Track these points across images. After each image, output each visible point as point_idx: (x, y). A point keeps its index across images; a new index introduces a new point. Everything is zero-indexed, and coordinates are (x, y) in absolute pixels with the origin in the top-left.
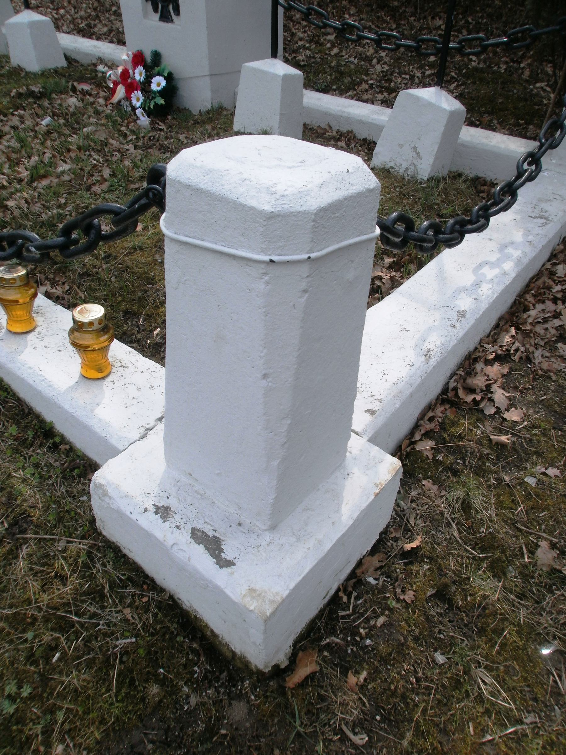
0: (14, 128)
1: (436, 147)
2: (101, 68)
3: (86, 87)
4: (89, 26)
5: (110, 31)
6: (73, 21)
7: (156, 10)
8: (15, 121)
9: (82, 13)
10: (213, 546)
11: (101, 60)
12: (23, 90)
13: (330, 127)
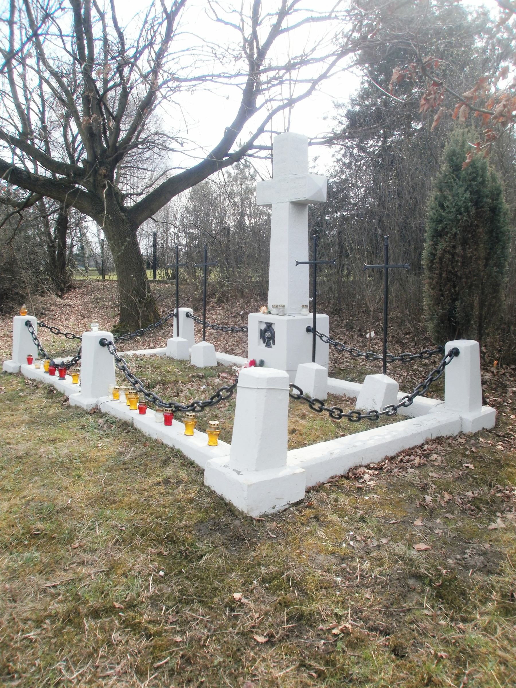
0: (189, 389)
1: (382, 399)
2: (234, 368)
3: (225, 375)
4: (232, 349)
5: (243, 352)
6: (224, 347)
7: (264, 342)
8: (189, 386)
9: (230, 343)
10: (239, 473)
11: (235, 364)
12: (195, 374)
13: (345, 396)
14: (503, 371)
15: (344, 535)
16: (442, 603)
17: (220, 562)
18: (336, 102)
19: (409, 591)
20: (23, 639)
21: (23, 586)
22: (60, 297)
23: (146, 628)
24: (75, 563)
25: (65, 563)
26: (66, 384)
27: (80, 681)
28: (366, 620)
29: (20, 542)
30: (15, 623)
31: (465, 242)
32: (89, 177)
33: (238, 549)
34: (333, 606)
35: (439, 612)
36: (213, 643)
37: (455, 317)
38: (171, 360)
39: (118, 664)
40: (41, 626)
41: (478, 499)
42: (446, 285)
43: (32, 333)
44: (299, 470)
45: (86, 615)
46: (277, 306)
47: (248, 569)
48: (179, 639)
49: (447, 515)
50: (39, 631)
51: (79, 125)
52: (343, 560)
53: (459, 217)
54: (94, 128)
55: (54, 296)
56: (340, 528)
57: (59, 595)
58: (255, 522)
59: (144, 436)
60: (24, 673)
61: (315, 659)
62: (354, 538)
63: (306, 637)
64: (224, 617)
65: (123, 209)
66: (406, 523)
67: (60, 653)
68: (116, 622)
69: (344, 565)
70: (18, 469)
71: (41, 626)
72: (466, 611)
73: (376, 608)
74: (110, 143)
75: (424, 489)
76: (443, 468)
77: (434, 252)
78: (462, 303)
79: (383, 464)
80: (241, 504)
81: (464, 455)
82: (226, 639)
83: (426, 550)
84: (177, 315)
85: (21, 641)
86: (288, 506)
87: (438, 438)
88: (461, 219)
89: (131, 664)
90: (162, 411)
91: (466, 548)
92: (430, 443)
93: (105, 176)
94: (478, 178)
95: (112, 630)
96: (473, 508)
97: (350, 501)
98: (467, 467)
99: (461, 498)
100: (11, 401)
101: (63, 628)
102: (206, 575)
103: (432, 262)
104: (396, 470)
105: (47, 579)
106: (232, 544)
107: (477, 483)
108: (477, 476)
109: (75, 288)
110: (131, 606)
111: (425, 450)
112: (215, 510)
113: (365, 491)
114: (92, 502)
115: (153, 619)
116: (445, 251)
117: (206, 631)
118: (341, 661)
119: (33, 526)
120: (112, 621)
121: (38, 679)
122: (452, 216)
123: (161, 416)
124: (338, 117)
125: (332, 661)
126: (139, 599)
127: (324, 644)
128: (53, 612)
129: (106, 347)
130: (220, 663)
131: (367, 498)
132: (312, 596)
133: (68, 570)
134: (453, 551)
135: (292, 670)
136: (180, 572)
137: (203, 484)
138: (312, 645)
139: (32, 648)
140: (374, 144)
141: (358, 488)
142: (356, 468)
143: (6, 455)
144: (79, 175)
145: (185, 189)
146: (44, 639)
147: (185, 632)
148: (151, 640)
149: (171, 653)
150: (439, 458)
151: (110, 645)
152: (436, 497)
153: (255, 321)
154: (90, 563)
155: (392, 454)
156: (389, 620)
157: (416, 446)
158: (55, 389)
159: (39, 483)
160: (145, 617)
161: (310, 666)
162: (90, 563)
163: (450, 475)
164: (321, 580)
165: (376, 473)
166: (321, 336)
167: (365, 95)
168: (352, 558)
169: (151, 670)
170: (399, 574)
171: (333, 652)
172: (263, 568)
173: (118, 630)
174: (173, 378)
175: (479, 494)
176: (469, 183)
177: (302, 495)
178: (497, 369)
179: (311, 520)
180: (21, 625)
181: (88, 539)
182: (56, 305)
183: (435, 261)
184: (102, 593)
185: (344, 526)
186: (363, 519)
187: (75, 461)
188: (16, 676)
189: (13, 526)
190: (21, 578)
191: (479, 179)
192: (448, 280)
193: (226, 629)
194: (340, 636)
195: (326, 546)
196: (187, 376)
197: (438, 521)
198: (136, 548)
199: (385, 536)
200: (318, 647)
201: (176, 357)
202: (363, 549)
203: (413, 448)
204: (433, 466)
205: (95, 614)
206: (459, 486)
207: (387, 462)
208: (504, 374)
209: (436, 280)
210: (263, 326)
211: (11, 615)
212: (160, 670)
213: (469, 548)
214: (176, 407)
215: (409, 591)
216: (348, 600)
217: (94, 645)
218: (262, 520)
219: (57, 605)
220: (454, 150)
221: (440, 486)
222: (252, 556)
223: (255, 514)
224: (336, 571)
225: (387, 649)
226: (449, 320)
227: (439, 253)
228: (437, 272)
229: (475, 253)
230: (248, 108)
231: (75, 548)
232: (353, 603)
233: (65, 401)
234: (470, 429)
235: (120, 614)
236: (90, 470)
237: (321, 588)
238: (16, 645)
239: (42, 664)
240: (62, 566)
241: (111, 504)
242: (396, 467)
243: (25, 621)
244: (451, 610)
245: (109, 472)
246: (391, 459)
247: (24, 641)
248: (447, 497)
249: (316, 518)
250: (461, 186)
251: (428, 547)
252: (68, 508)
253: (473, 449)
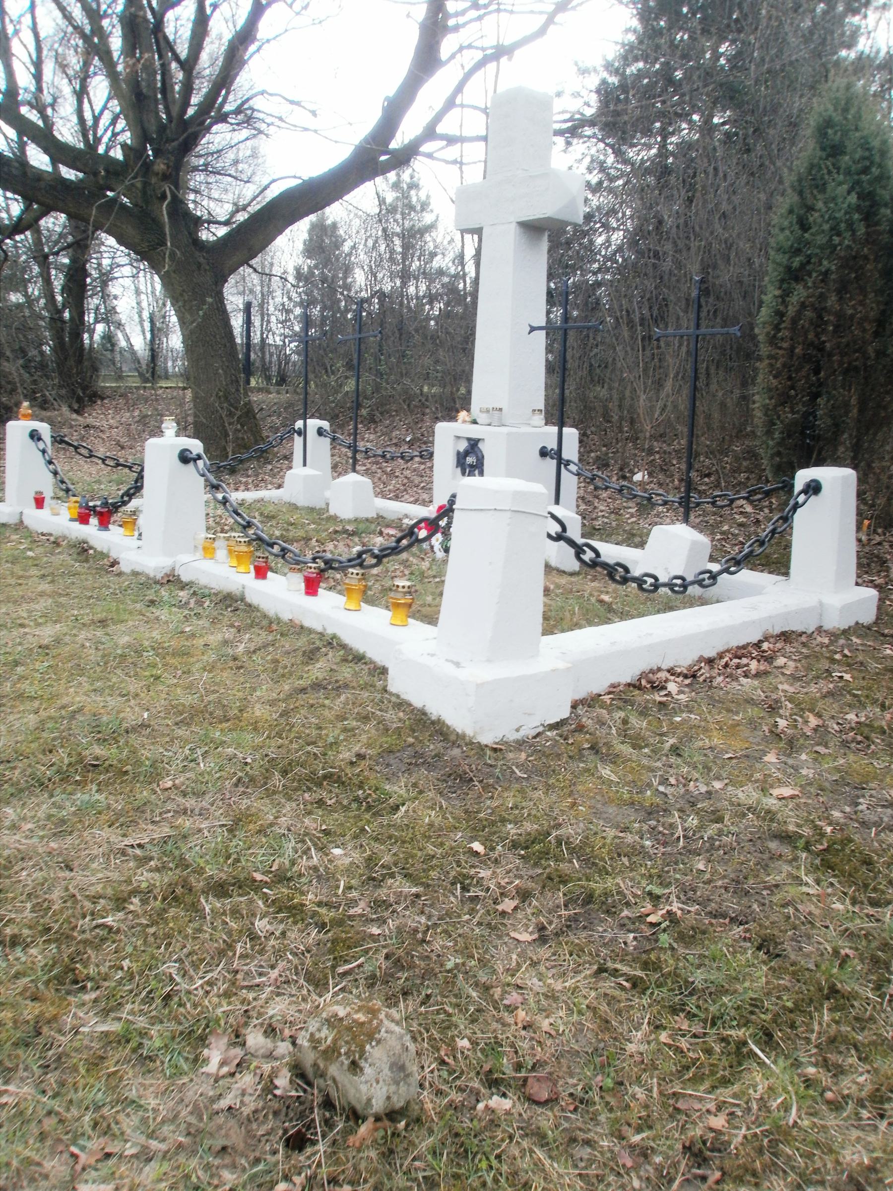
10: (457, 664)
12: (339, 528)
14: (878, 539)
15: (646, 777)
16: (835, 876)
17: (430, 816)
18: (580, 64)
19: (771, 858)
20: (96, 927)
21: (82, 846)
22: (77, 412)
23: (315, 914)
24: (169, 811)
25: (152, 811)
26: (110, 540)
27: (207, 992)
28: (704, 902)
29: (65, 779)
30: (76, 902)
31: (842, 290)
32: (135, 178)
33: (462, 796)
34: (644, 883)
35: (830, 890)
36: (438, 936)
37: (813, 427)
38: (293, 507)
39: (273, 967)
40: (124, 908)
41: (867, 725)
42: (798, 371)
43: (44, 452)
44: (561, 665)
45: (203, 892)
46: (488, 411)
47: (484, 827)
48: (375, 931)
49: (818, 748)
50: (120, 915)
51: (113, 75)
52: (650, 814)
53: (836, 240)
54: (143, 84)
55: (65, 409)
56: (639, 765)
57: (151, 859)
58: (488, 752)
59: (265, 616)
60: (105, 980)
61: (622, 961)
62: (664, 781)
63: (601, 929)
64: (452, 899)
65: (197, 243)
66: (752, 758)
67: (166, 949)
68: (260, 903)
69: (653, 823)
70: (46, 664)
71: (124, 908)
72: (875, 890)
73: (720, 883)
74: (175, 110)
75: (773, 708)
76: (799, 679)
77: (782, 308)
78: (828, 401)
79: (696, 668)
80: (459, 720)
81: (833, 661)
82: (460, 931)
83: (792, 797)
84: (302, 433)
85: (92, 930)
86: (541, 729)
87: (783, 634)
88: (840, 244)
89: (296, 968)
90: (300, 570)
91: (858, 797)
92: (771, 640)
93: (165, 177)
94: (874, 169)
95: (254, 915)
96: (859, 738)
97: (649, 723)
98: (841, 677)
99: (838, 724)
100: (12, 563)
101: (165, 910)
102: (410, 835)
103: (777, 328)
104: (720, 679)
105: (124, 835)
106: (450, 787)
107: (860, 701)
108: (859, 692)
109: (103, 399)
110: (281, 878)
111: (764, 651)
112: (414, 731)
113: (673, 708)
114: (185, 718)
115: (325, 900)
116: (803, 306)
117: (423, 919)
118: (671, 962)
119: (87, 752)
120: (251, 901)
121: (131, 991)
122: (821, 240)
123: (297, 581)
124: (584, 93)
125: (654, 963)
126: (295, 868)
127: (635, 938)
128: (144, 885)
129: (192, 463)
130: (457, 965)
131: (678, 719)
132: (604, 867)
133: (159, 822)
134: (837, 800)
135: (585, 978)
136: (363, 830)
137: (385, 690)
138: (614, 940)
139: (114, 942)
140: (642, 153)
141: (660, 703)
142: (652, 671)
143: (20, 644)
144: (115, 172)
145: (301, 217)
146: (133, 927)
147: (385, 922)
148: (326, 933)
149: (366, 951)
150: (791, 664)
151: (253, 937)
152: (795, 721)
153: (447, 437)
154: (197, 811)
155: (711, 653)
156: (744, 901)
157: (748, 644)
158: (91, 548)
159: (87, 687)
160: (310, 896)
161: (616, 970)
162: (197, 811)
163: (813, 688)
164: (617, 844)
165: (687, 681)
166: (568, 463)
167: (630, 55)
168: (665, 811)
169: (333, 978)
170: (751, 833)
171: (653, 949)
172: (509, 826)
173: (264, 916)
174: (301, 533)
175: (867, 717)
176: (856, 177)
177: (565, 713)
178: (868, 535)
179: (586, 753)
180: (88, 905)
181: (188, 775)
182: (71, 427)
183: (783, 325)
184: (228, 857)
185: (645, 761)
186: (676, 751)
187: (145, 654)
188: (89, 985)
189: (51, 751)
190: (76, 833)
191: (875, 171)
192: (806, 358)
193: (459, 916)
194: (663, 926)
195: (618, 791)
196: (327, 530)
197: (804, 757)
198: (274, 793)
199: (718, 778)
200: (625, 943)
201: (302, 502)
202: (683, 796)
203: (744, 647)
204: (783, 674)
205: (220, 889)
206: (831, 707)
207: (703, 665)
208: (879, 544)
209: (781, 360)
210: (463, 446)
211: (67, 889)
212: (350, 978)
213: (864, 796)
214: (327, 562)
215: (771, 858)
216: (668, 872)
217: (225, 937)
218: (501, 750)
219: (150, 875)
220: (830, 117)
221: (799, 704)
222: (488, 807)
223: (487, 739)
224: (641, 831)
225: (749, 944)
226: (802, 433)
227: (791, 311)
228: (785, 345)
229: (860, 308)
230: (427, 60)
231: (166, 789)
232: (678, 876)
233: (112, 565)
234: (835, 621)
235: (265, 890)
236: (176, 668)
237: (619, 855)
238: (84, 936)
239: (135, 967)
240: (148, 815)
241: (221, 722)
242: (719, 675)
243: (95, 899)
244: (850, 886)
245: (210, 671)
246: (710, 661)
247: (97, 931)
248: (813, 721)
249: (594, 748)
250: (840, 184)
251: (797, 793)
252: (144, 726)
253: (846, 652)
